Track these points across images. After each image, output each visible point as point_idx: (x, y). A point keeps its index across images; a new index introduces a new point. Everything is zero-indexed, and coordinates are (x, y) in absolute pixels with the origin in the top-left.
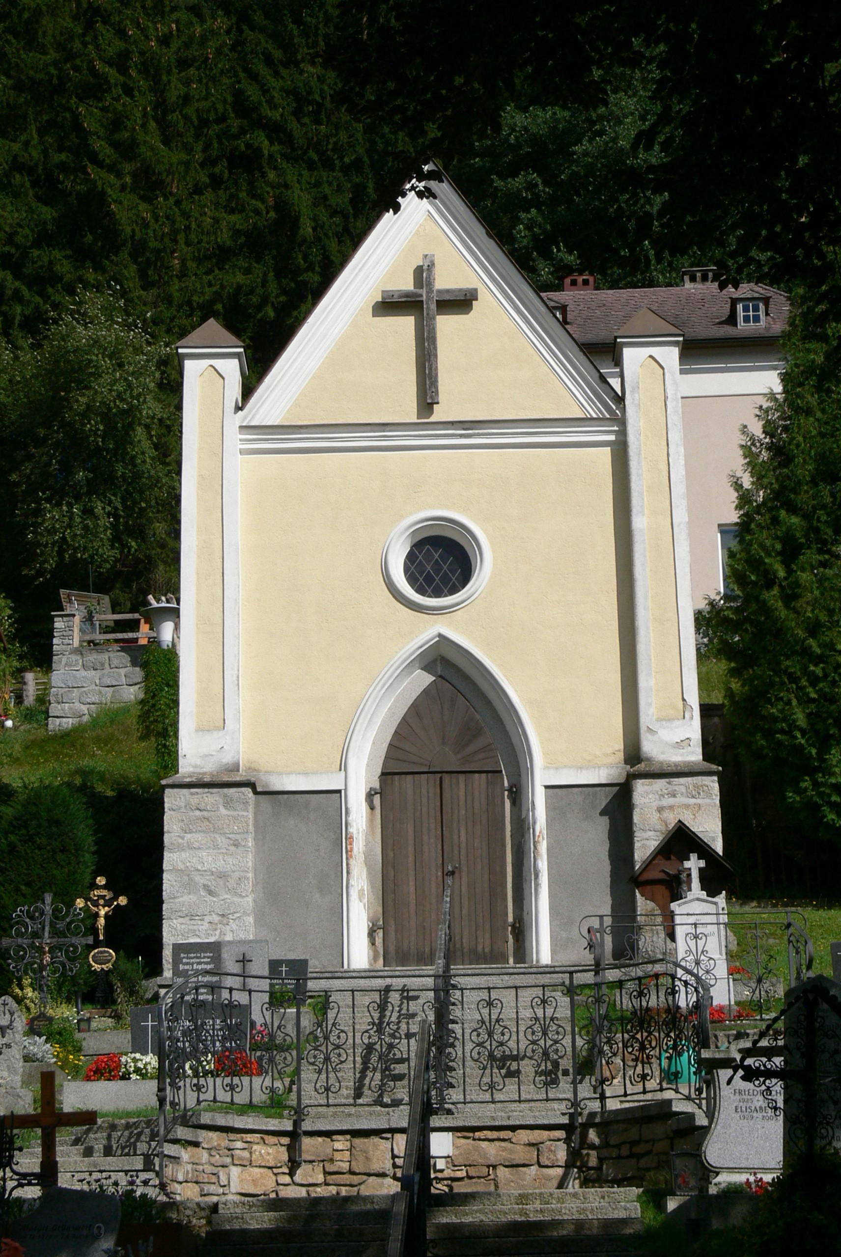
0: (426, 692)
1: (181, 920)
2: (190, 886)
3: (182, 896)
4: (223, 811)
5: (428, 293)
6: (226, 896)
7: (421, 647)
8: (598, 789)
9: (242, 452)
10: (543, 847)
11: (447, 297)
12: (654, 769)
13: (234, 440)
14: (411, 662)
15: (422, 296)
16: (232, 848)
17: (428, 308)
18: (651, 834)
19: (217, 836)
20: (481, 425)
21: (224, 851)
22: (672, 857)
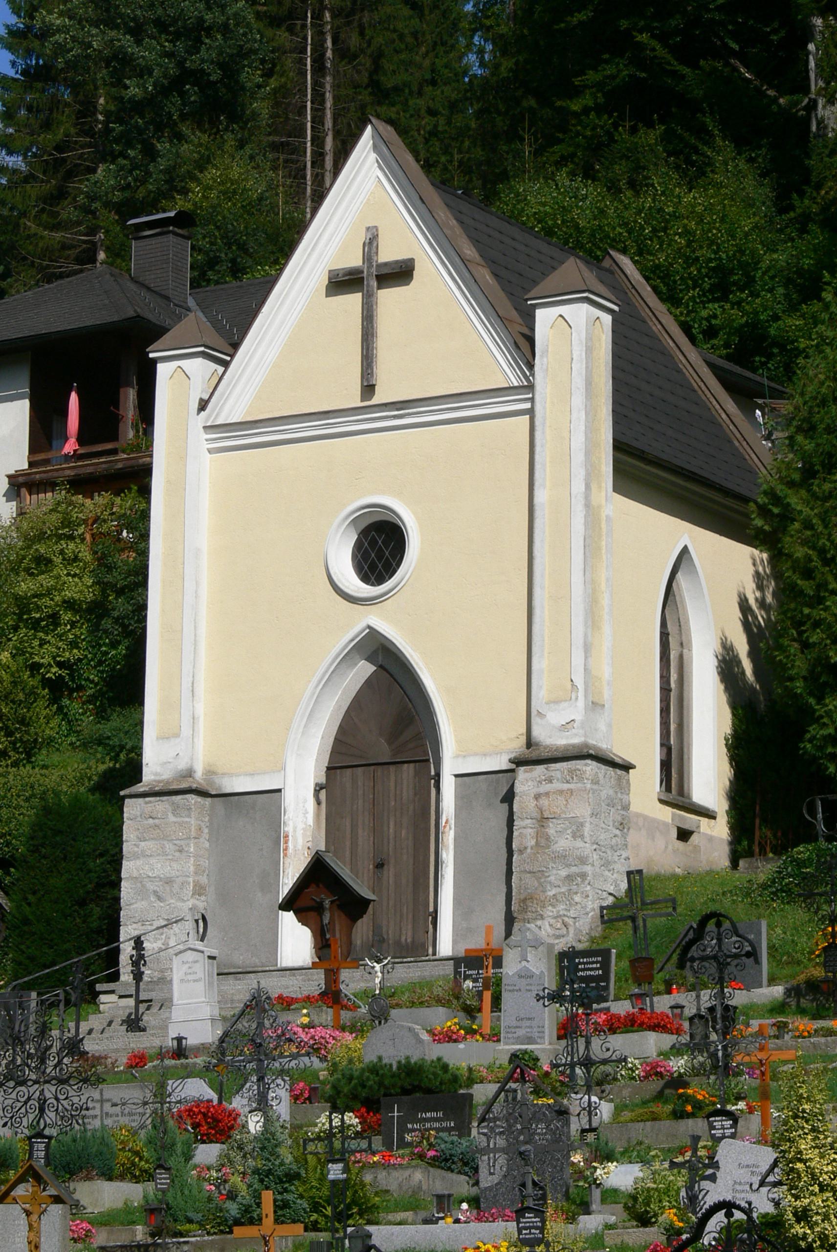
0: (368, 683)
1: (134, 926)
2: (142, 893)
3: (136, 903)
4: (172, 818)
5: (368, 267)
6: (172, 901)
7: (352, 640)
8: (501, 775)
9: (210, 451)
10: (449, 838)
12: (545, 755)
13: (200, 441)
14: (346, 655)
15: (362, 272)
16: (177, 854)
17: (368, 285)
18: (528, 822)
19: (165, 843)
20: (411, 405)
21: (170, 857)
22: (321, 886)
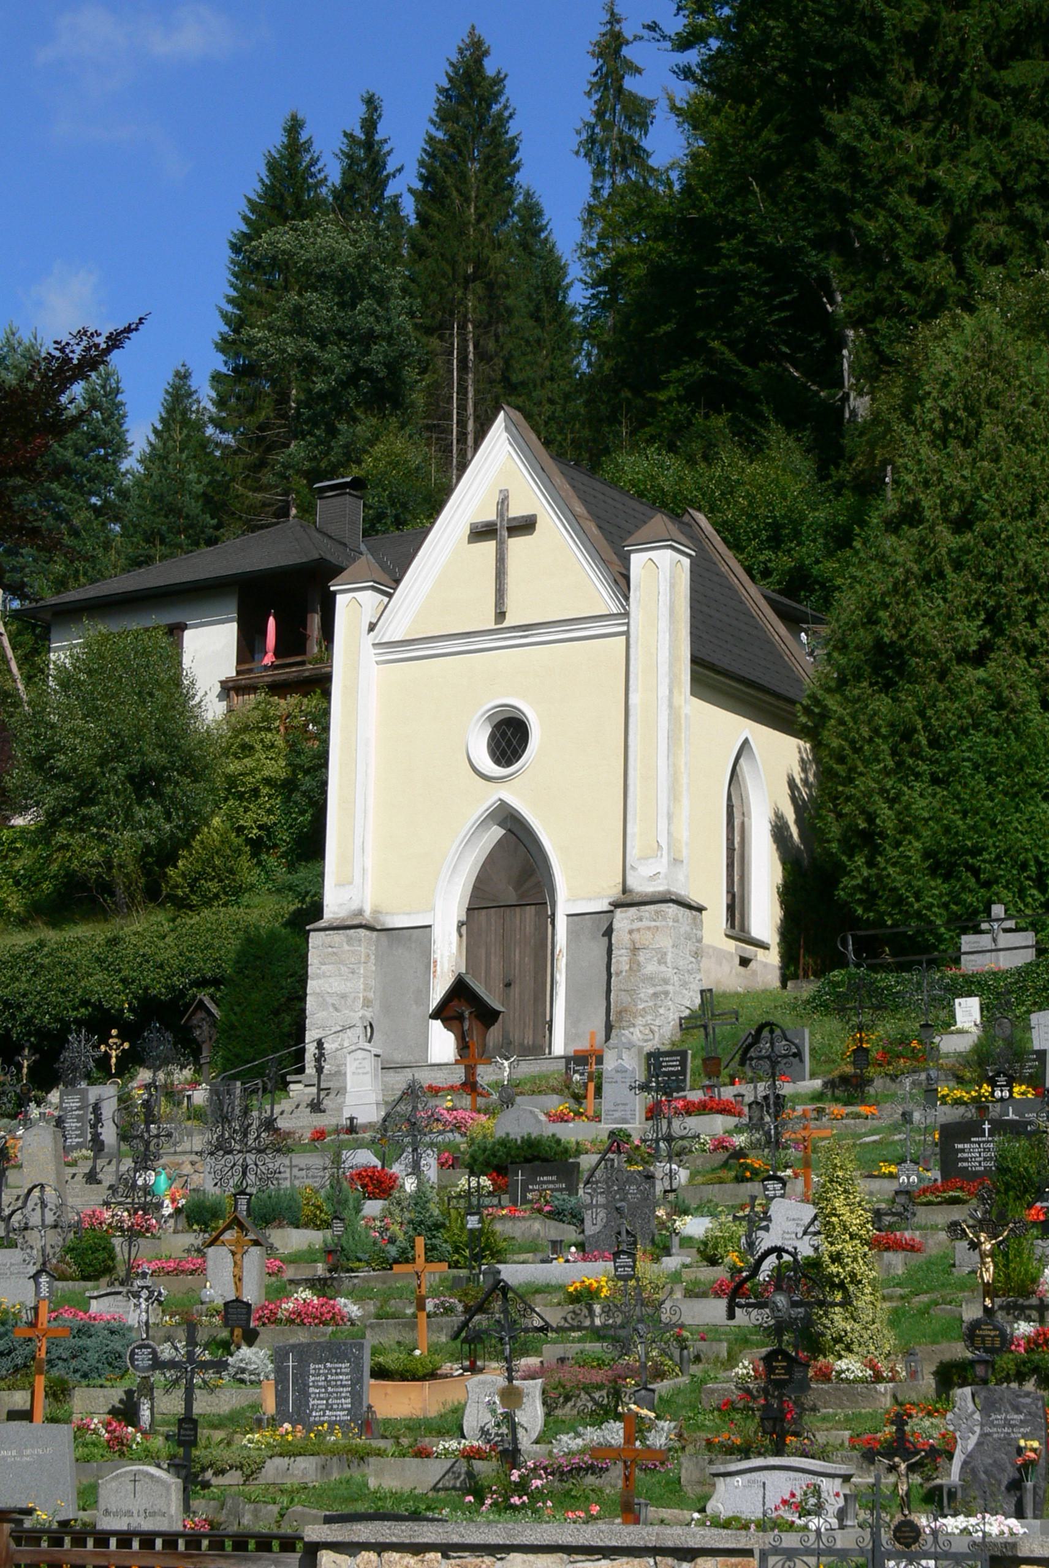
0: (499, 842)
2: (323, 1005)
4: (346, 947)
9: (377, 663)
10: (562, 963)
11: (514, 524)
12: (637, 899)
13: (369, 655)
